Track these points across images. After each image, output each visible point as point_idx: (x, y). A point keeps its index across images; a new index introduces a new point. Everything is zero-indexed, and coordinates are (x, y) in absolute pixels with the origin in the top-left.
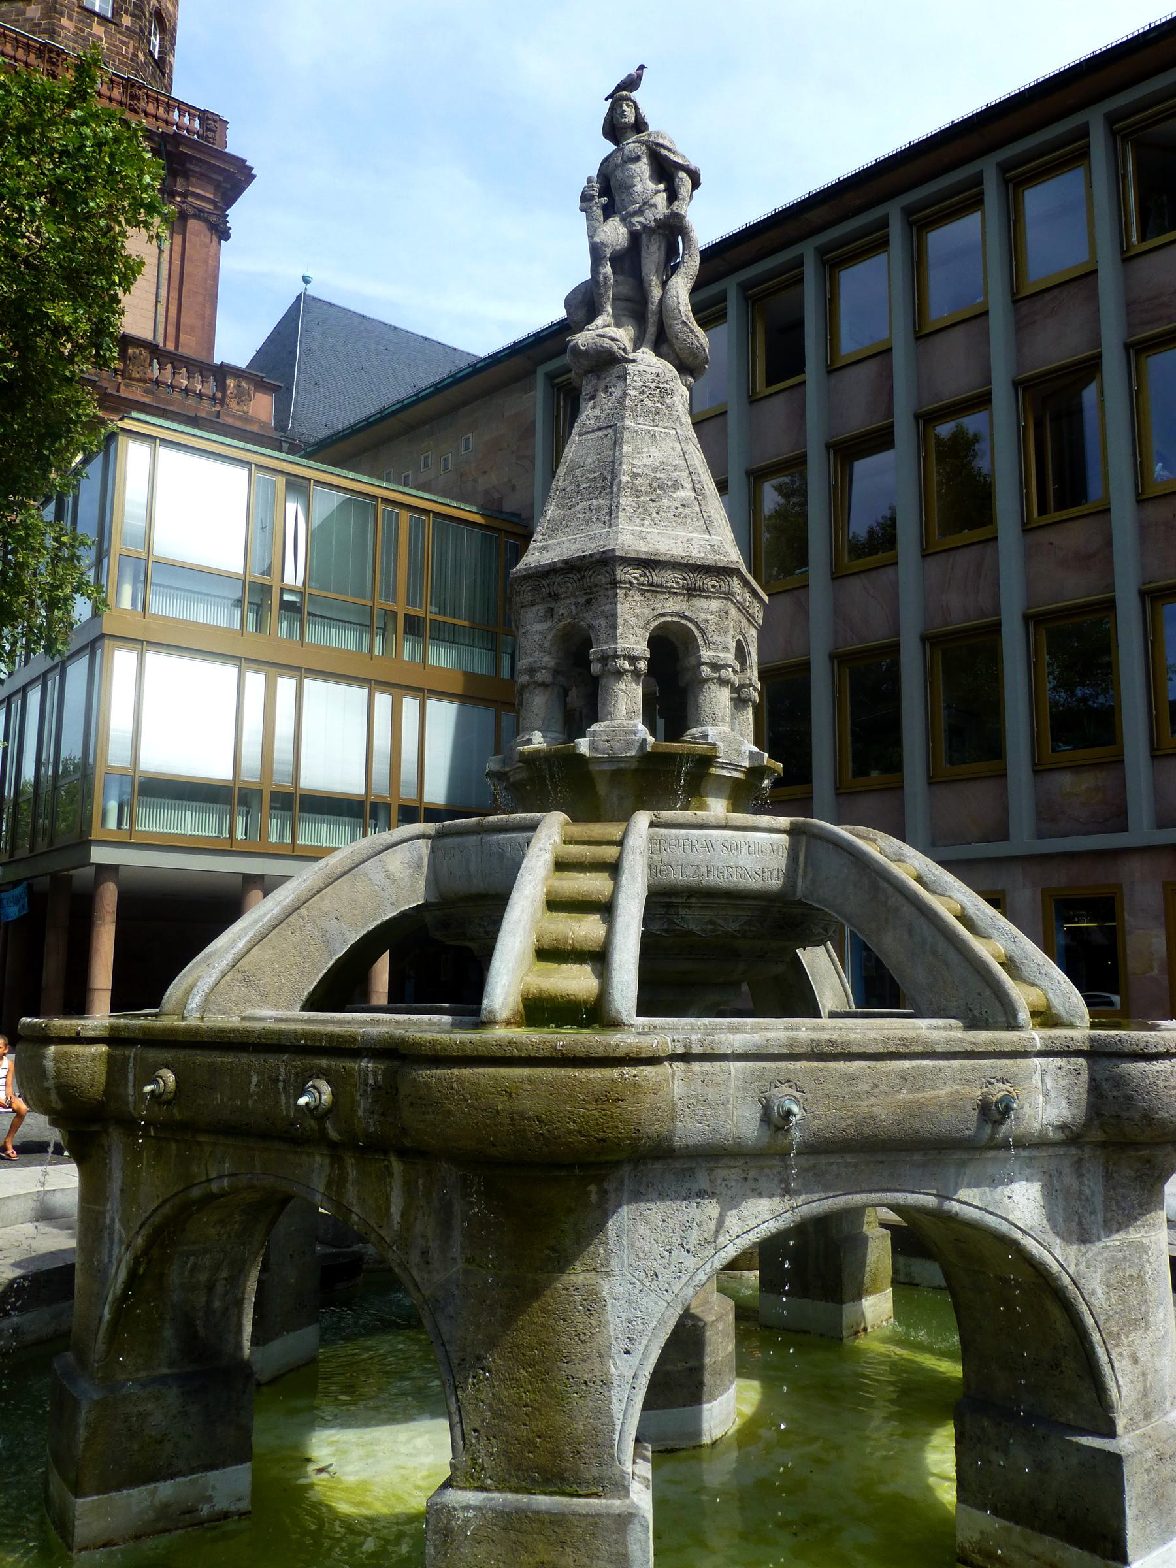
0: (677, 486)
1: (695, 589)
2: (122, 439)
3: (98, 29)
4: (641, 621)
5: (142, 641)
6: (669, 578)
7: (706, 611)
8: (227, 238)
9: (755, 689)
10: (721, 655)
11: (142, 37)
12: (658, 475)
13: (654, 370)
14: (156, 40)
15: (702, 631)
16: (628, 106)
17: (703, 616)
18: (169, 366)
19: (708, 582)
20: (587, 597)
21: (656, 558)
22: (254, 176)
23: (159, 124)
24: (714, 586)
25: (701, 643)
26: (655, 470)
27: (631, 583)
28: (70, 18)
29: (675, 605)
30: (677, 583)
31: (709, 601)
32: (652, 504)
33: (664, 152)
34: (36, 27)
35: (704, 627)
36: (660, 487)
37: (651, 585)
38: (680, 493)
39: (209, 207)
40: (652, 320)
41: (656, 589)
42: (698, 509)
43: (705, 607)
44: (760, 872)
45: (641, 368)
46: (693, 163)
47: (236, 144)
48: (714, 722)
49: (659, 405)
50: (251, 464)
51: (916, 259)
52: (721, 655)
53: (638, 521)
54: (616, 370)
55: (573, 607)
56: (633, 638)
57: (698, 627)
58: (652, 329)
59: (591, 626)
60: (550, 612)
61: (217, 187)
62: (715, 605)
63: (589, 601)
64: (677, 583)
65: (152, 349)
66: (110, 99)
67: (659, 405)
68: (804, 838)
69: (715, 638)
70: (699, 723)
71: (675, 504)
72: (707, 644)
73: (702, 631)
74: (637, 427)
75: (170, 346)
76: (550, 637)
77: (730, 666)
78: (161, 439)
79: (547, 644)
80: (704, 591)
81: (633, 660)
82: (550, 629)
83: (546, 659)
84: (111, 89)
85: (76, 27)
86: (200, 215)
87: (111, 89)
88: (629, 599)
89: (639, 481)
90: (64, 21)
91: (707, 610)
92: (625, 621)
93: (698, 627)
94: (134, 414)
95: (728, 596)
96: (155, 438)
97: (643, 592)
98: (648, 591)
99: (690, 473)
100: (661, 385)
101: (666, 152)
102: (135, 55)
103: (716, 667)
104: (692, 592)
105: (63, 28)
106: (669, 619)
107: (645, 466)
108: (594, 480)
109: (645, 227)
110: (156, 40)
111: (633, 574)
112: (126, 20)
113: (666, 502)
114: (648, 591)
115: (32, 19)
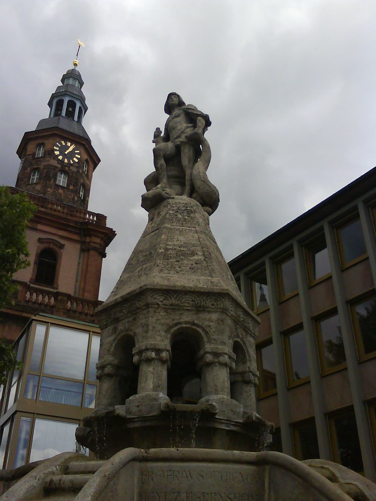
0: (193, 254)
1: (200, 307)
2: (34, 322)
3: (61, 191)
4: (165, 328)
5: (34, 413)
6: (187, 301)
7: (209, 320)
8: (105, 257)
9: (254, 375)
10: (220, 347)
11: (77, 192)
12: (182, 249)
13: (184, 202)
14: (82, 193)
15: (207, 333)
16: (175, 97)
17: (207, 323)
18: (75, 303)
19: (209, 303)
20: (134, 317)
21: (174, 288)
22: (116, 234)
23: (80, 219)
24: (213, 305)
25: (205, 339)
26: (180, 247)
27: (158, 304)
28: (51, 188)
29: (187, 318)
30: (188, 303)
31: (211, 314)
32: (176, 263)
33: (190, 111)
34: (39, 192)
35: (208, 330)
36: (182, 255)
37: (172, 305)
38: (196, 257)
39: (98, 246)
40: (188, 183)
41: (174, 308)
42: (205, 265)
43: (208, 317)
44: (231, 496)
45: (177, 201)
46: (205, 112)
47: (109, 224)
48: (216, 392)
49: (186, 217)
50: (90, 331)
51: (372, 219)
52: (220, 347)
53: (166, 271)
54: (165, 203)
55: (126, 324)
56: (159, 338)
57: (204, 330)
58: (188, 188)
59: (135, 334)
60: (115, 329)
61: (102, 239)
62: (214, 316)
63: (135, 319)
64: (188, 303)
65: (69, 297)
66: (63, 213)
67: (186, 217)
68: (267, 467)
69: (215, 337)
70: (208, 393)
71: (192, 263)
72: (209, 341)
73: (207, 333)
74: (172, 227)
75: (81, 297)
76: (114, 345)
77: (226, 354)
78: (51, 323)
79: (112, 349)
80: (207, 308)
81: (158, 351)
82: (115, 339)
83: (112, 358)
84: (64, 210)
85: (53, 191)
86: (95, 249)
87: (64, 210)
88: (157, 314)
89: (170, 252)
90: (49, 189)
91: (209, 320)
92: (154, 327)
93: (204, 330)
94: (41, 314)
95: (224, 311)
96: (48, 323)
97: (166, 310)
98: (170, 309)
99: (202, 248)
100: (188, 208)
101: (192, 111)
102: (74, 198)
103: (216, 354)
104: (199, 309)
105: (48, 191)
106: (184, 326)
107: (174, 245)
108: (146, 255)
109: (182, 142)
110: (82, 193)
111: (159, 299)
112: (71, 187)
113: (185, 262)
114: (170, 309)
115: (38, 190)
